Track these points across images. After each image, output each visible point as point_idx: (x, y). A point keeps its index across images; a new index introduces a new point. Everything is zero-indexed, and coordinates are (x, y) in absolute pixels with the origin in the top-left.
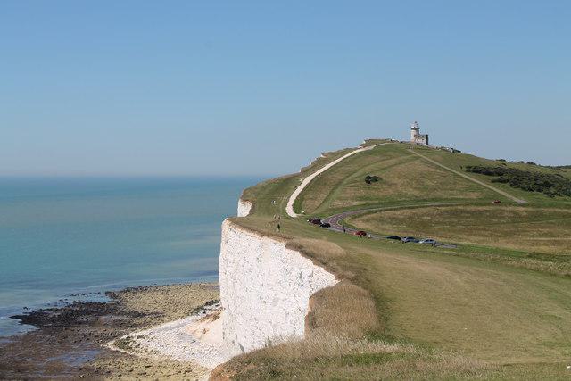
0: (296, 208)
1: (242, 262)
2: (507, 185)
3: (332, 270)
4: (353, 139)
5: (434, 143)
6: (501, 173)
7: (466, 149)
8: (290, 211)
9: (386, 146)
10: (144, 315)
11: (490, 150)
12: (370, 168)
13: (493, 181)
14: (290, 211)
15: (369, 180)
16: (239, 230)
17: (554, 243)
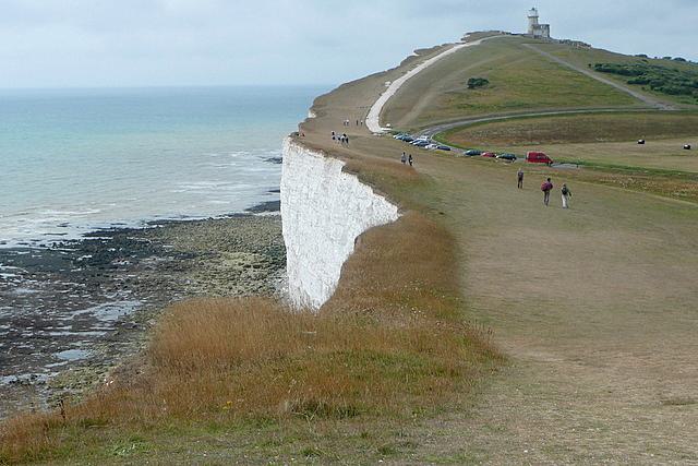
0: (384, 118)
1: (305, 190)
2: (648, 87)
3: (393, 199)
4: (448, 32)
5: (555, 35)
6: (638, 72)
7: (597, 41)
8: (373, 124)
9: (496, 40)
10: (195, 256)
11: (625, 44)
12: (474, 69)
13: (630, 83)
14: (373, 124)
15: (475, 84)
16: (301, 149)
17: (249, 172)
